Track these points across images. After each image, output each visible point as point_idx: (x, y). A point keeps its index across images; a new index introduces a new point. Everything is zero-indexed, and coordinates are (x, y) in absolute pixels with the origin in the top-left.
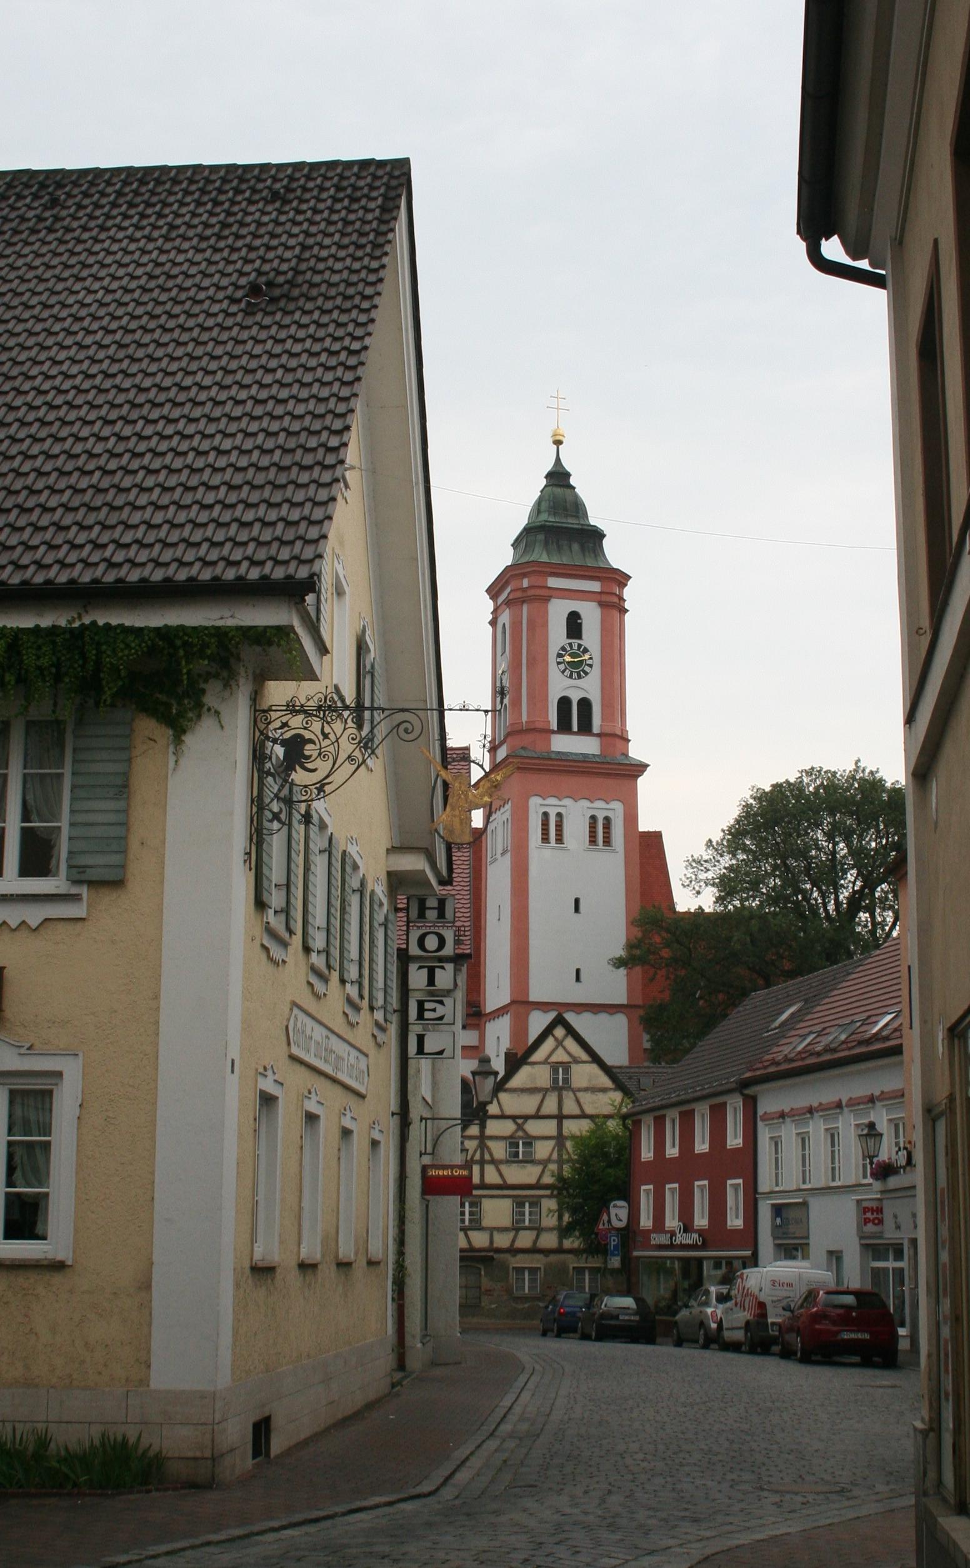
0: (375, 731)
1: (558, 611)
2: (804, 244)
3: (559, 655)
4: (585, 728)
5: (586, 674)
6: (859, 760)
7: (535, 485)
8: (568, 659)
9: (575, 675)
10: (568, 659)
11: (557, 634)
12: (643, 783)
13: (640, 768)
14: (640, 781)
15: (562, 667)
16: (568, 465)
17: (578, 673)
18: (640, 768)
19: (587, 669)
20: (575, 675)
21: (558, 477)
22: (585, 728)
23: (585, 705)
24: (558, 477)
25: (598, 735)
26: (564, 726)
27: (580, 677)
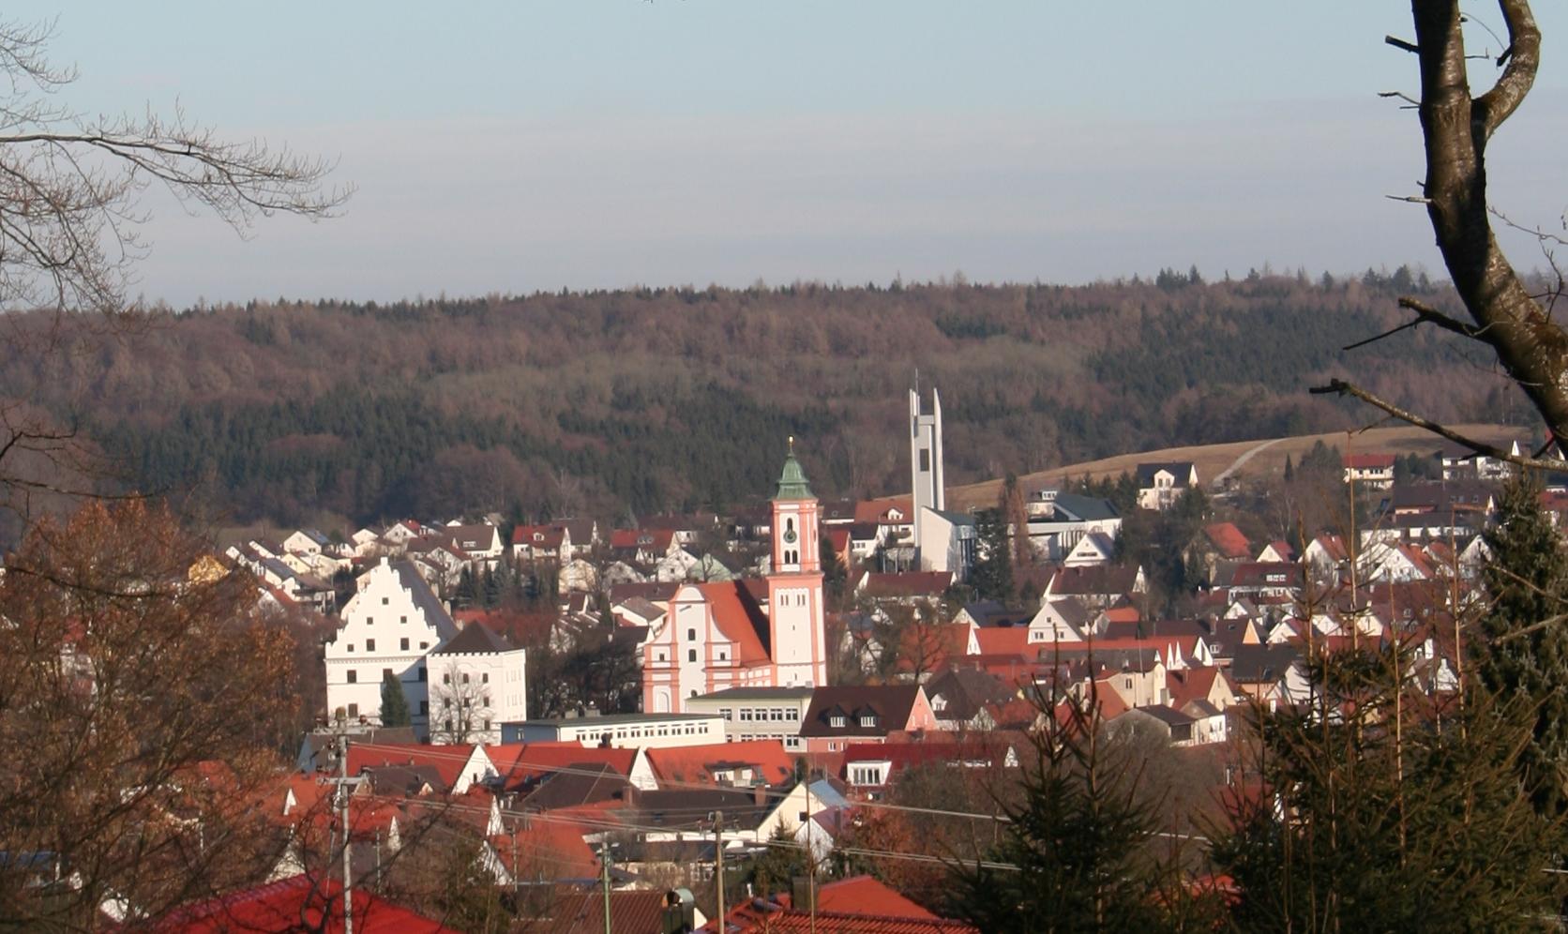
22: (795, 561)
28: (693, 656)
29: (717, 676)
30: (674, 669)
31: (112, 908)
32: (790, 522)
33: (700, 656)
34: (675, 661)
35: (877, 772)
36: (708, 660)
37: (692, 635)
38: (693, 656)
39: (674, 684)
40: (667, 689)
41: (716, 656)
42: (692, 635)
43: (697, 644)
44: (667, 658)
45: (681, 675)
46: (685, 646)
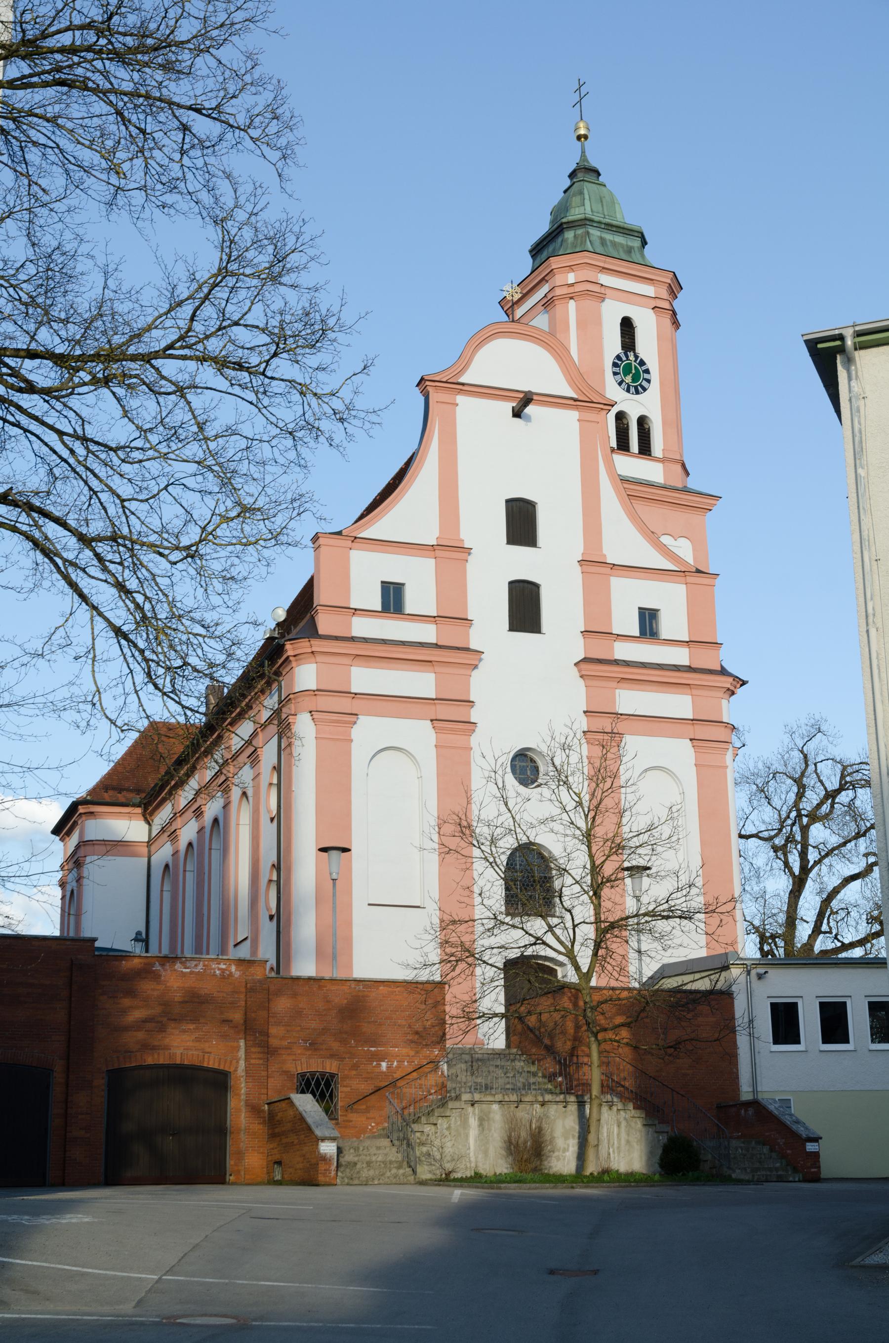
4: (645, 449)
5: (645, 389)
11: (613, 345)
19: (645, 384)
20: (632, 390)
25: (657, 460)
27: (637, 393)
28: (525, 607)
29: (630, 700)
30: (453, 654)
33: (561, 607)
37: (521, 523)
38: (525, 607)
39: (451, 717)
40: (419, 735)
42: (521, 523)
43: (551, 566)
44: (420, 597)
45: (479, 685)
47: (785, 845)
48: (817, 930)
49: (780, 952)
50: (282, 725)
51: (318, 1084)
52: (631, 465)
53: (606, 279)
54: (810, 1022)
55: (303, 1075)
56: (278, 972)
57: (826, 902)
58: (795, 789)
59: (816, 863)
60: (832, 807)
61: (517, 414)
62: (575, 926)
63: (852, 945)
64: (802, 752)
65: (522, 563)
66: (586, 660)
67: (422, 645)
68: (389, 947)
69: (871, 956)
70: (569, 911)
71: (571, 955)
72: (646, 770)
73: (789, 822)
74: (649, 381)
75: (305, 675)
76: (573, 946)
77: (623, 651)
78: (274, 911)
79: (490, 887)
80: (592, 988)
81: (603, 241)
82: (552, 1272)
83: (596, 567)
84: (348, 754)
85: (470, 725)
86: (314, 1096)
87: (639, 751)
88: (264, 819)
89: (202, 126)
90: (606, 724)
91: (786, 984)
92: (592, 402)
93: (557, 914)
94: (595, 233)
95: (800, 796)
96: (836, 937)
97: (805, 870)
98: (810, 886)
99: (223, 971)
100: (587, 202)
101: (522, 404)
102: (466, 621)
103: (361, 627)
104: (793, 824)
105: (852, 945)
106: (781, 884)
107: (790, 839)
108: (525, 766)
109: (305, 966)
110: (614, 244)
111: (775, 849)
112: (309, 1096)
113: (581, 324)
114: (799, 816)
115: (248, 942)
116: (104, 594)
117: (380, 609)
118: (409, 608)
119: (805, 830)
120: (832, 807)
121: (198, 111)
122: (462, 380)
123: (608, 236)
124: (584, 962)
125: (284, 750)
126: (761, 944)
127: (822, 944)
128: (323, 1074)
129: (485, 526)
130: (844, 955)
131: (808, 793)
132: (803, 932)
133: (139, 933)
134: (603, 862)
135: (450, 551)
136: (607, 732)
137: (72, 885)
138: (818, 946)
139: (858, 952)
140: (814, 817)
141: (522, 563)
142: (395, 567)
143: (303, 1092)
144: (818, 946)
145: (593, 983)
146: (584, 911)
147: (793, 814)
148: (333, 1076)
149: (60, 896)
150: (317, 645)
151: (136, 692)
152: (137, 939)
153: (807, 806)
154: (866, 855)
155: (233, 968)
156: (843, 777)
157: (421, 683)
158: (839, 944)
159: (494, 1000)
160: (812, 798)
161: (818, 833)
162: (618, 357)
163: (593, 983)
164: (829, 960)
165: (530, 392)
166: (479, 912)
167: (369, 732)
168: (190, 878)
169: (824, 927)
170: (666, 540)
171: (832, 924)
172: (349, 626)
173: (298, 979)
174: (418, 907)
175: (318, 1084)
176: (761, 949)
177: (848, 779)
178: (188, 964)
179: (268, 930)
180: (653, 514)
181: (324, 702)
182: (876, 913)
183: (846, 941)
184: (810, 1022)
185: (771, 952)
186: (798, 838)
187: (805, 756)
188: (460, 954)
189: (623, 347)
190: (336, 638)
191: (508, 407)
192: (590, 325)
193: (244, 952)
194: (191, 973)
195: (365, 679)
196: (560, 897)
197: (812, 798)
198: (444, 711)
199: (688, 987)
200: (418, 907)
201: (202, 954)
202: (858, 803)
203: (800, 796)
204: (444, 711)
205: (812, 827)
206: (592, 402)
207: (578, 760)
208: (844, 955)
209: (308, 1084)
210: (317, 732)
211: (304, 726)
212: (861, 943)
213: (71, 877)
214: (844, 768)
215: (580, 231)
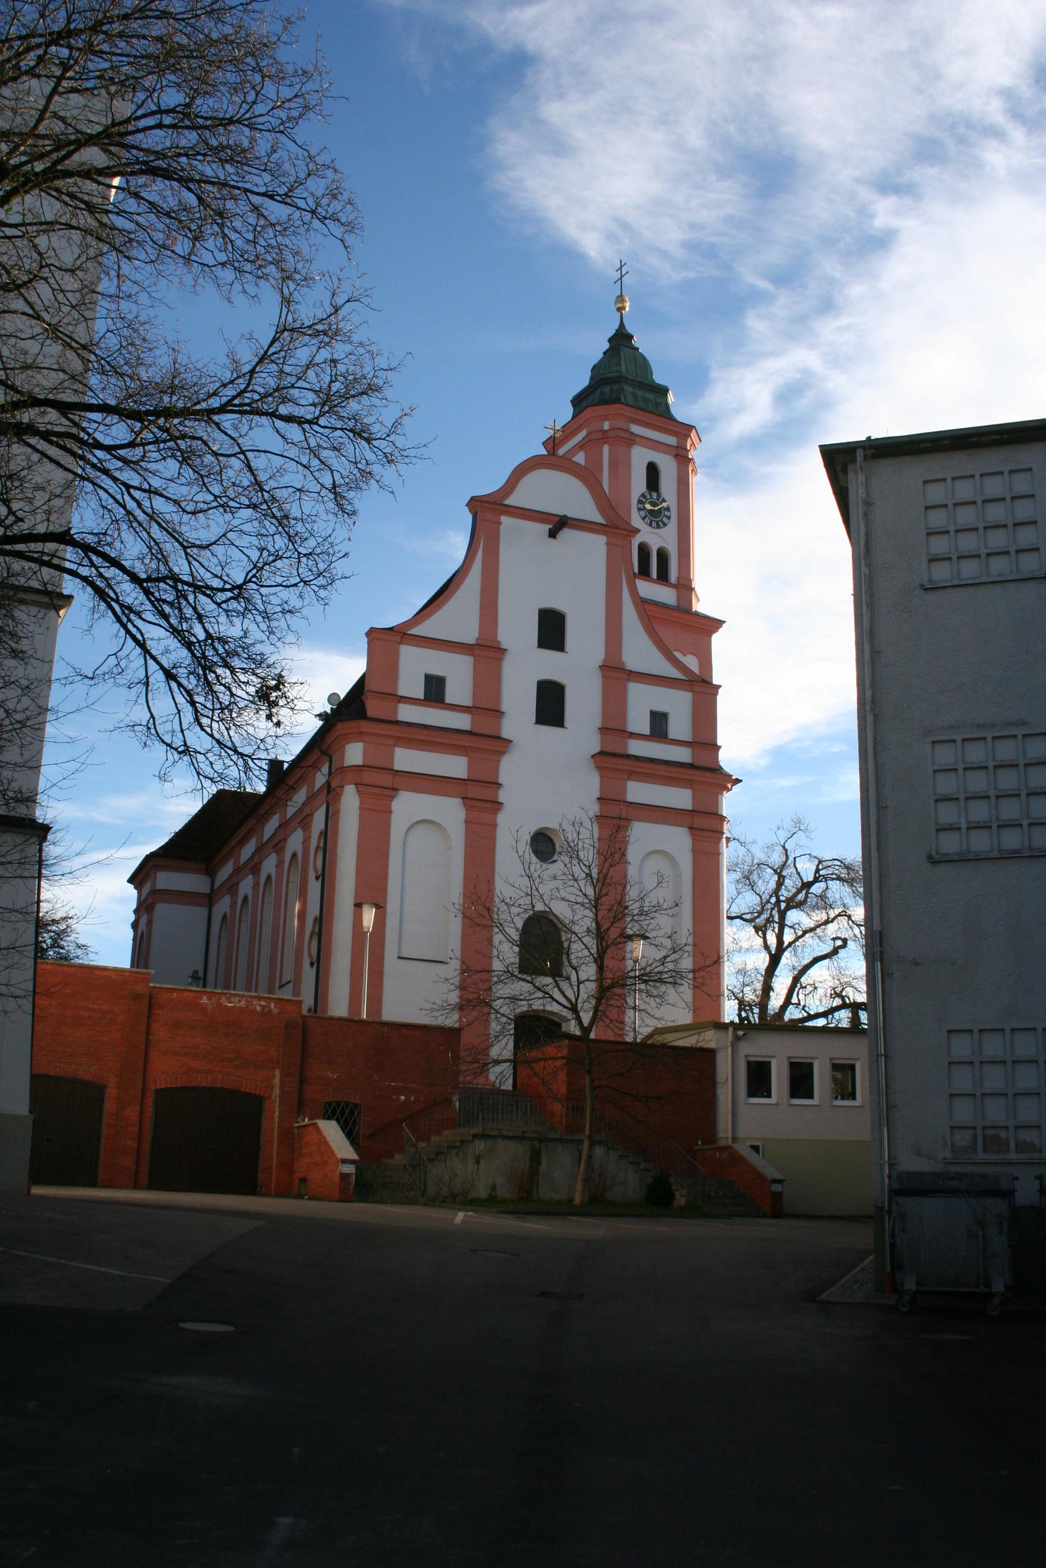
0: (240, 750)
1: (640, 457)
2: (721, 764)
3: (640, 502)
4: (663, 577)
5: (665, 525)
6: (922, 586)
7: (595, 346)
8: (648, 507)
9: (654, 524)
10: (648, 507)
11: (639, 483)
12: (718, 641)
13: (714, 624)
14: (716, 638)
15: (643, 513)
16: (630, 329)
17: (657, 523)
18: (714, 624)
19: (665, 520)
20: (654, 524)
21: (621, 339)
22: (663, 577)
23: (663, 556)
24: (621, 339)
25: (674, 586)
26: (644, 572)
27: (658, 527)
28: (550, 705)
29: (639, 792)
30: (485, 742)
31: (403, 1098)
32: (72, 741)
33: (583, 705)
34: (487, 709)
35: (985, 1151)
36: (613, 728)
37: (552, 630)
38: (550, 705)
39: (481, 798)
40: (450, 811)
41: (639, 722)
42: (552, 630)
43: (577, 668)
44: (458, 691)
45: (508, 770)
46: (525, 667)
47: (765, 926)
48: (788, 1002)
49: (755, 1018)
50: (331, 792)
51: (343, 1112)
52: (648, 589)
53: (635, 429)
54: (779, 1078)
55: (329, 1104)
56: (316, 1011)
57: (796, 980)
58: (776, 877)
59: (790, 944)
60: (806, 897)
61: (553, 534)
62: (579, 983)
63: (818, 1016)
64: (784, 847)
65: (550, 665)
66: (601, 753)
67: (458, 731)
68: (417, 994)
69: (832, 1025)
70: (575, 969)
71: (574, 1009)
72: (644, 857)
73: (769, 906)
74: (669, 518)
75: (354, 754)
76: (577, 999)
77: (637, 748)
78: (315, 959)
79: (505, 952)
80: (592, 1040)
81: (635, 396)
82: (542, 1294)
83: (615, 674)
84: (387, 825)
85: (497, 806)
86: (339, 1122)
87: (643, 837)
88: (312, 875)
89: (276, 211)
90: (614, 811)
91: (760, 1047)
92: (618, 528)
93: (564, 973)
94: (629, 389)
95: (780, 884)
96: (803, 1009)
97: (781, 949)
98: (787, 958)
99: (263, 1007)
100: (623, 364)
101: (558, 525)
102: (499, 785)
103: (406, 713)
104: (772, 909)
105: (818, 1016)
106: (762, 960)
107: (769, 921)
108: (543, 844)
109: (338, 1006)
110: (645, 399)
111: (757, 929)
112: (334, 1123)
113: (614, 466)
114: (778, 901)
115: (291, 985)
116: (157, 636)
117: (422, 697)
118: (449, 699)
119: (782, 915)
120: (806, 897)
121: (271, 197)
122: (507, 502)
123: (640, 393)
124: (586, 1018)
125: (332, 818)
126: (740, 1010)
127: (793, 1014)
128: (347, 1104)
129: (518, 631)
130: (810, 1024)
131: (787, 882)
132: (776, 1002)
133: (196, 972)
134: (609, 928)
135: (487, 652)
136: (615, 818)
137: (142, 926)
138: (787, 1017)
139: (821, 1022)
140: (793, 903)
141: (550, 665)
142: (438, 663)
143: (329, 1118)
144: (787, 1017)
145: (592, 1036)
146: (589, 971)
147: (773, 900)
148: (356, 1106)
149: (132, 937)
150: (365, 726)
151: (182, 731)
152: (195, 977)
153: (784, 894)
154: (834, 939)
155: (272, 1005)
156: (817, 871)
157: (455, 766)
158: (805, 1014)
159: (503, 1048)
160: (791, 885)
161: (793, 916)
162: (643, 495)
163: (592, 1036)
164: (797, 1027)
165: (565, 516)
166: (497, 965)
167: (407, 806)
168: (245, 927)
169: (794, 1000)
170: (678, 655)
171: (801, 997)
172: (395, 712)
173: (331, 1018)
174: (442, 962)
175: (343, 1112)
176: (739, 1015)
177: (822, 873)
178: (232, 999)
179: (309, 974)
180: (668, 634)
181: (368, 777)
182: (838, 990)
183: (812, 1013)
184: (779, 1078)
185: (747, 1018)
186: (776, 919)
187: (786, 850)
188: (474, 997)
189: (648, 487)
190: (382, 721)
191: (546, 528)
192: (620, 467)
193: (287, 994)
194: (234, 1007)
195: (406, 759)
196: (568, 955)
197: (791, 885)
198: (474, 791)
199: (675, 1044)
200: (442, 962)
201: (250, 991)
202: (829, 894)
203: (780, 884)
204: (474, 791)
205: (789, 913)
206: (618, 528)
207: (589, 839)
208: (810, 1024)
209: (334, 1112)
210: (361, 802)
211: (350, 800)
212: (824, 1015)
213: (144, 919)
214: (820, 862)
215: (615, 387)
